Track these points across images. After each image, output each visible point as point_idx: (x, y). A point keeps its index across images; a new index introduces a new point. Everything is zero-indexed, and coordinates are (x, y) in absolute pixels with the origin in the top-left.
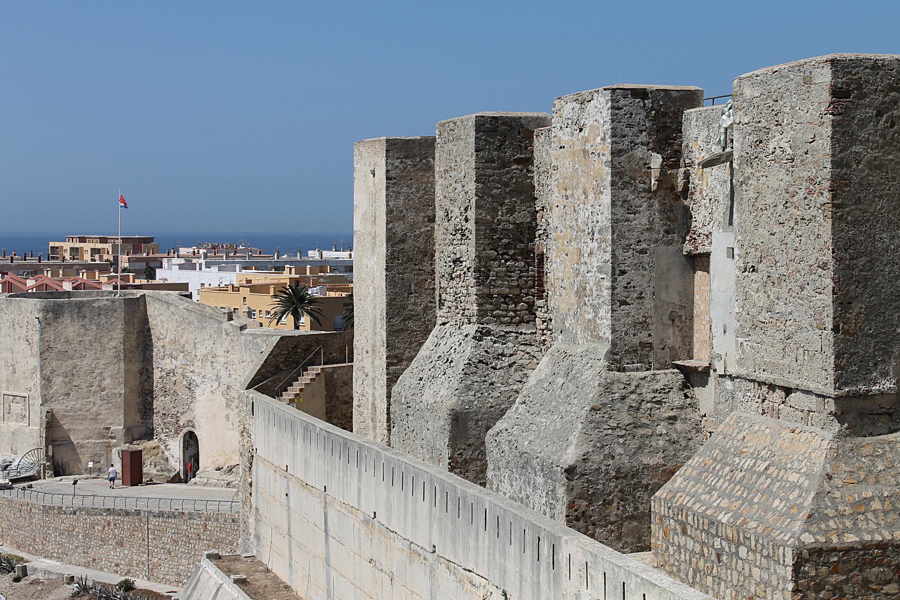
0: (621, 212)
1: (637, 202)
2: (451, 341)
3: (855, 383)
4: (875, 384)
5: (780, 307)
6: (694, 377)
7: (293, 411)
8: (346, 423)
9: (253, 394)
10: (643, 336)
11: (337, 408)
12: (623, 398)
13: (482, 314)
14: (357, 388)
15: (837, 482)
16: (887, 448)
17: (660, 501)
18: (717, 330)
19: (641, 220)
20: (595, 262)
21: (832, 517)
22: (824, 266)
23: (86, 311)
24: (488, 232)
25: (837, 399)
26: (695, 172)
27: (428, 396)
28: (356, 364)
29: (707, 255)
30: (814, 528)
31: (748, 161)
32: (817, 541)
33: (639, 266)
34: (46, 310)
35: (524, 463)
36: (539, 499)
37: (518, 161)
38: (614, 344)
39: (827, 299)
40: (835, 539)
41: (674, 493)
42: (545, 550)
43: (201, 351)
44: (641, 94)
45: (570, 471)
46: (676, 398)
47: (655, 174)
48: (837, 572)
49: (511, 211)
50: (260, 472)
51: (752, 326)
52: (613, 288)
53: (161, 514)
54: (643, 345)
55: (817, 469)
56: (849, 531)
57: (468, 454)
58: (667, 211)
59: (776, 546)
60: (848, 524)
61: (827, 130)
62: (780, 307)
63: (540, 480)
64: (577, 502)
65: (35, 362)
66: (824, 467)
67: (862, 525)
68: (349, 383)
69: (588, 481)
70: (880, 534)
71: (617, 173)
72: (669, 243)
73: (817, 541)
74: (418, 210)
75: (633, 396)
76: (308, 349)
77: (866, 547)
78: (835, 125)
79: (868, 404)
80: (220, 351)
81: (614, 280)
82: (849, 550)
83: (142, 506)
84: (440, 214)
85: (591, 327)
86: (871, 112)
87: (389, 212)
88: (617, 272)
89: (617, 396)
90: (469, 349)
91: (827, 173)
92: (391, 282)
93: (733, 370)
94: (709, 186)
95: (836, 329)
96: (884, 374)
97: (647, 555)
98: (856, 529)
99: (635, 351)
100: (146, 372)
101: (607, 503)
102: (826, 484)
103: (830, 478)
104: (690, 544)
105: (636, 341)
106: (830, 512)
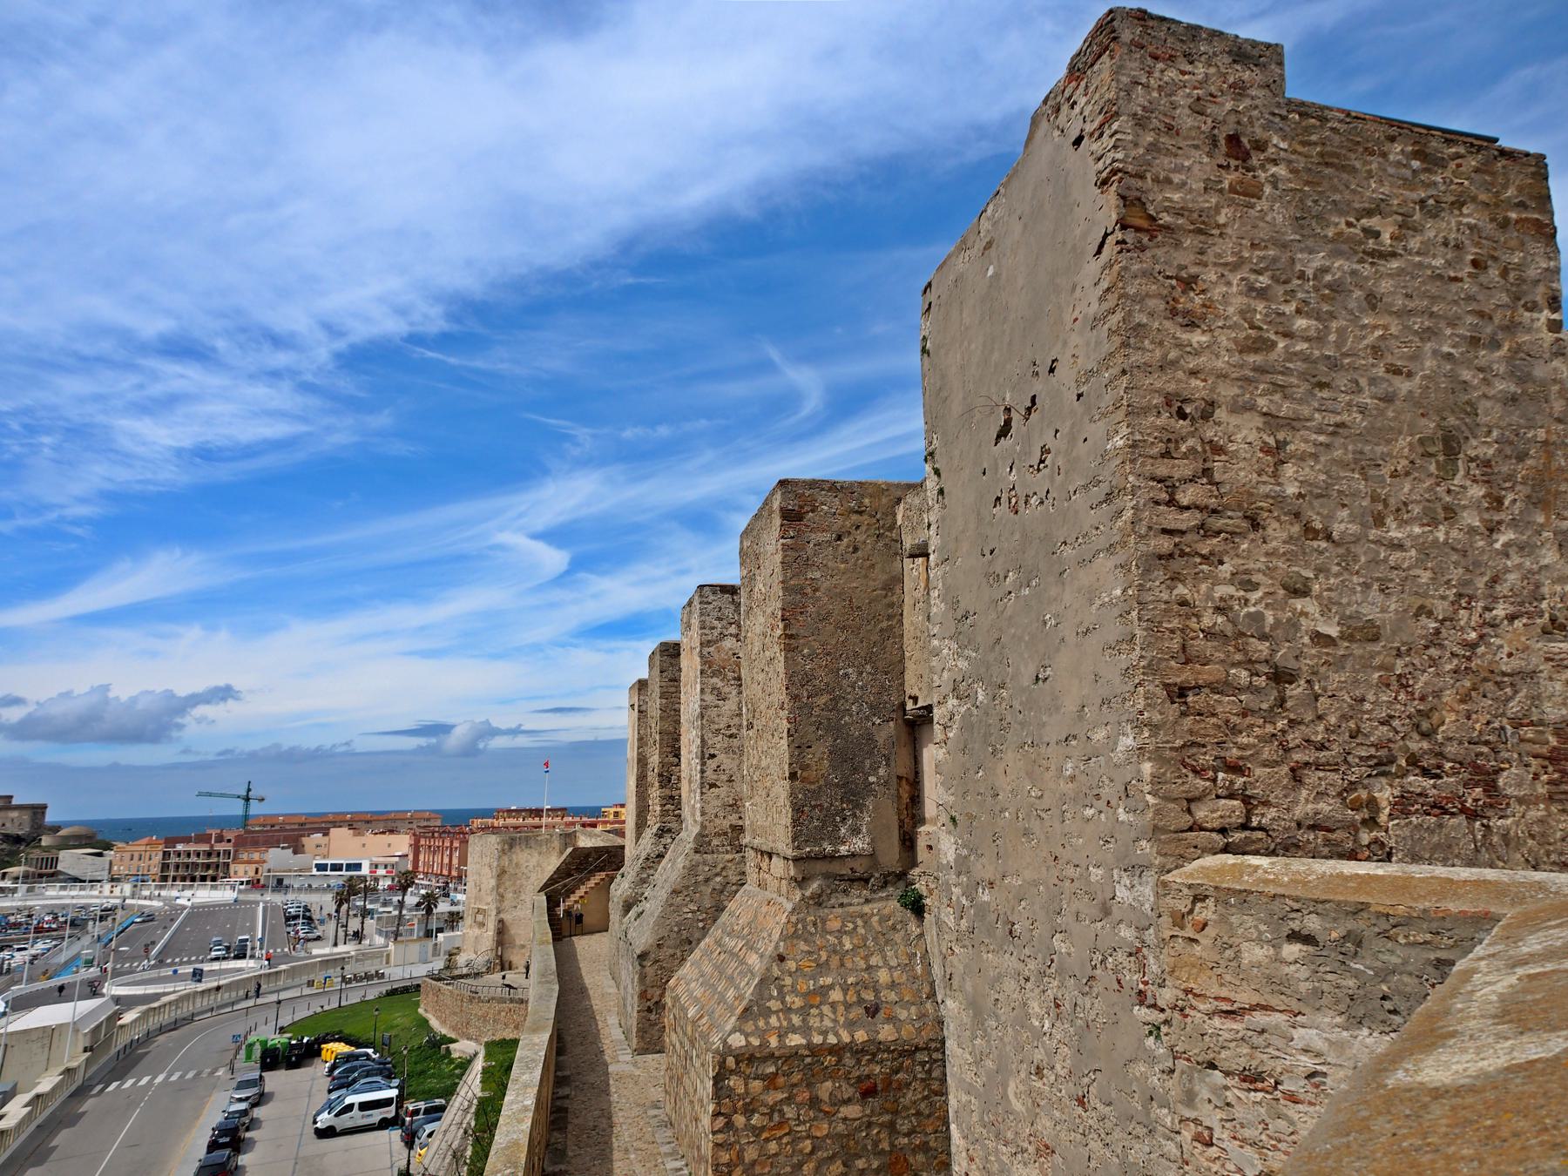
0: (710, 698)
1: (726, 689)
3: (817, 842)
4: (844, 843)
12: (707, 880)
15: (791, 965)
16: (860, 922)
21: (776, 1012)
23: (532, 843)
25: (796, 860)
30: (749, 1027)
32: (748, 1044)
33: (728, 750)
34: (504, 842)
38: (703, 827)
40: (774, 1042)
48: (776, 1089)
52: (702, 772)
54: (733, 827)
56: (794, 1030)
60: (796, 1020)
64: (650, 991)
65: (493, 882)
66: (777, 947)
67: (814, 1022)
69: (662, 968)
70: (836, 1034)
73: (748, 1044)
75: (718, 879)
78: (785, 548)
79: (836, 868)
81: (703, 764)
82: (793, 1055)
89: (701, 878)
95: (793, 776)
96: (856, 831)
98: (805, 1030)
99: (725, 834)
102: (775, 968)
103: (782, 958)
105: (726, 824)
106: (774, 1005)
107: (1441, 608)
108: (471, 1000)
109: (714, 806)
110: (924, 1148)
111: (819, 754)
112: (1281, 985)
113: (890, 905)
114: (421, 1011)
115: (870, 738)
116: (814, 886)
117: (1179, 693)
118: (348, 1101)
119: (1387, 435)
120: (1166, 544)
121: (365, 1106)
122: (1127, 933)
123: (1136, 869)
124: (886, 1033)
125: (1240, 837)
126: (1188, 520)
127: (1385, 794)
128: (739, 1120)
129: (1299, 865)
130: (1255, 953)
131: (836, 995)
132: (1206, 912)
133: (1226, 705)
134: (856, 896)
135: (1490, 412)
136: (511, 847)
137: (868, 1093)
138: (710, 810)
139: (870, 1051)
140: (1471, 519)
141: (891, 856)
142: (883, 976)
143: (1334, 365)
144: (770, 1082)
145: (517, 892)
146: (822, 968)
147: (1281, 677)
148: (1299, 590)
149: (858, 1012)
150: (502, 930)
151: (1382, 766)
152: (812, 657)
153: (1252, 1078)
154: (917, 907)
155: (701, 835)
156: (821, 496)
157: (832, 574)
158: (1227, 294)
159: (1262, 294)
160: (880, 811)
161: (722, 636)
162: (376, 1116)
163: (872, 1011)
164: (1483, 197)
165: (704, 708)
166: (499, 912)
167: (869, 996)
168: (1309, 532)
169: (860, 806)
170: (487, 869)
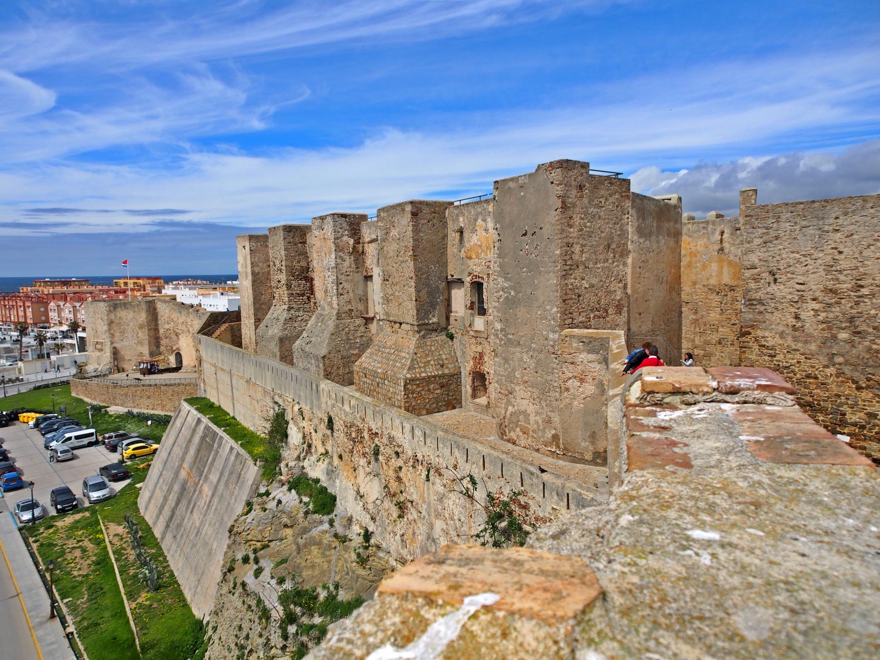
0: (339, 261)
2: (279, 311)
5: (397, 294)
6: (368, 320)
7: (217, 341)
8: (240, 345)
9: (200, 336)
10: (349, 307)
11: (237, 341)
13: (290, 301)
14: (243, 331)
17: (356, 368)
18: (376, 304)
19: (347, 264)
20: (330, 280)
22: (411, 278)
23: (128, 306)
24: (291, 271)
26: (366, 245)
27: (270, 333)
28: (242, 323)
29: (371, 276)
31: (383, 240)
33: (346, 281)
35: (307, 355)
36: (313, 368)
37: (301, 243)
39: (413, 290)
41: (361, 363)
42: (314, 386)
43: (180, 321)
44: (344, 216)
45: (324, 357)
46: (362, 329)
47: (351, 246)
49: (299, 262)
50: (205, 365)
51: (387, 300)
53: (166, 385)
55: (411, 351)
57: (286, 354)
58: (356, 261)
59: (398, 379)
61: (410, 228)
62: (397, 294)
63: (313, 361)
65: (106, 328)
68: (240, 330)
71: (337, 246)
72: (358, 272)
74: (264, 263)
76: (223, 318)
77: (429, 377)
78: (413, 226)
80: (189, 320)
82: (424, 378)
83: (158, 382)
84: (272, 263)
85: (330, 304)
86: (425, 221)
87: (252, 264)
88: (338, 283)
90: (285, 315)
91: (411, 244)
92: (254, 290)
93: (382, 317)
94: (371, 250)
95: (416, 300)
96: (434, 316)
97: (354, 387)
98: (426, 372)
100: (156, 330)
101: (338, 368)
104: (368, 381)
105: (347, 309)
106: (416, 366)
107: (604, 280)
108: (115, 387)
109: (342, 302)
110: (456, 399)
111: (424, 293)
112: (578, 349)
113: (443, 337)
114: (73, 394)
115: (438, 288)
116: (422, 333)
117: (564, 301)
118: (67, 435)
119: (598, 245)
120: (564, 273)
121: (77, 437)
122: (551, 343)
123: (555, 332)
124: (446, 371)
125: (572, 326)
126: (568, 267)
127: (592, 316)
128: (411, 396)
129: (582, 330)
130: (575, 345)
131: (432, 362)
132: (567, 339)
133: (571, 302)
134: (434, 334)
135: (616, 239)
136: (115, 309)
137: (442, 387)
138: (341, 304)
139: (443, 376)
140: (610, 261)
141: (443, 323)
142: (444, 357)
143: (592, 232)
144: (418, 386)
145: (122, 333)
146: (427, 355)
147: (579, 296)
148: (583, 279)
149: (438, 366)
150: (115, 353)
151: (592, 310)
152: (421, 262)
153: (572, 363)
154: (451, 337)
155: (338, 313)
156: (424, 207)
157: (426, 235)
158: (577, 220)
159: (582, 219)
160: (440, 309)
161: (342, 235)
162: (86, 441)
163: (442, 366)
164: (629, 291)
165: (337, 264)
166: (112, 343)
167: (441, 362)
168: (586, 267)
169: (435, 309)
170: (100, 321)
